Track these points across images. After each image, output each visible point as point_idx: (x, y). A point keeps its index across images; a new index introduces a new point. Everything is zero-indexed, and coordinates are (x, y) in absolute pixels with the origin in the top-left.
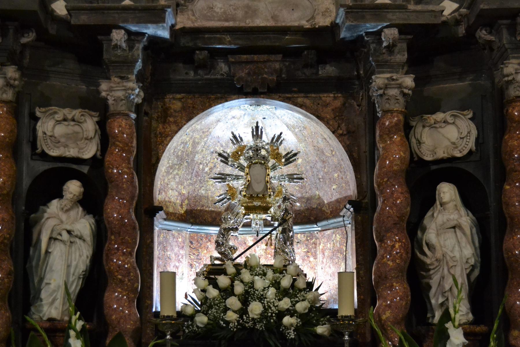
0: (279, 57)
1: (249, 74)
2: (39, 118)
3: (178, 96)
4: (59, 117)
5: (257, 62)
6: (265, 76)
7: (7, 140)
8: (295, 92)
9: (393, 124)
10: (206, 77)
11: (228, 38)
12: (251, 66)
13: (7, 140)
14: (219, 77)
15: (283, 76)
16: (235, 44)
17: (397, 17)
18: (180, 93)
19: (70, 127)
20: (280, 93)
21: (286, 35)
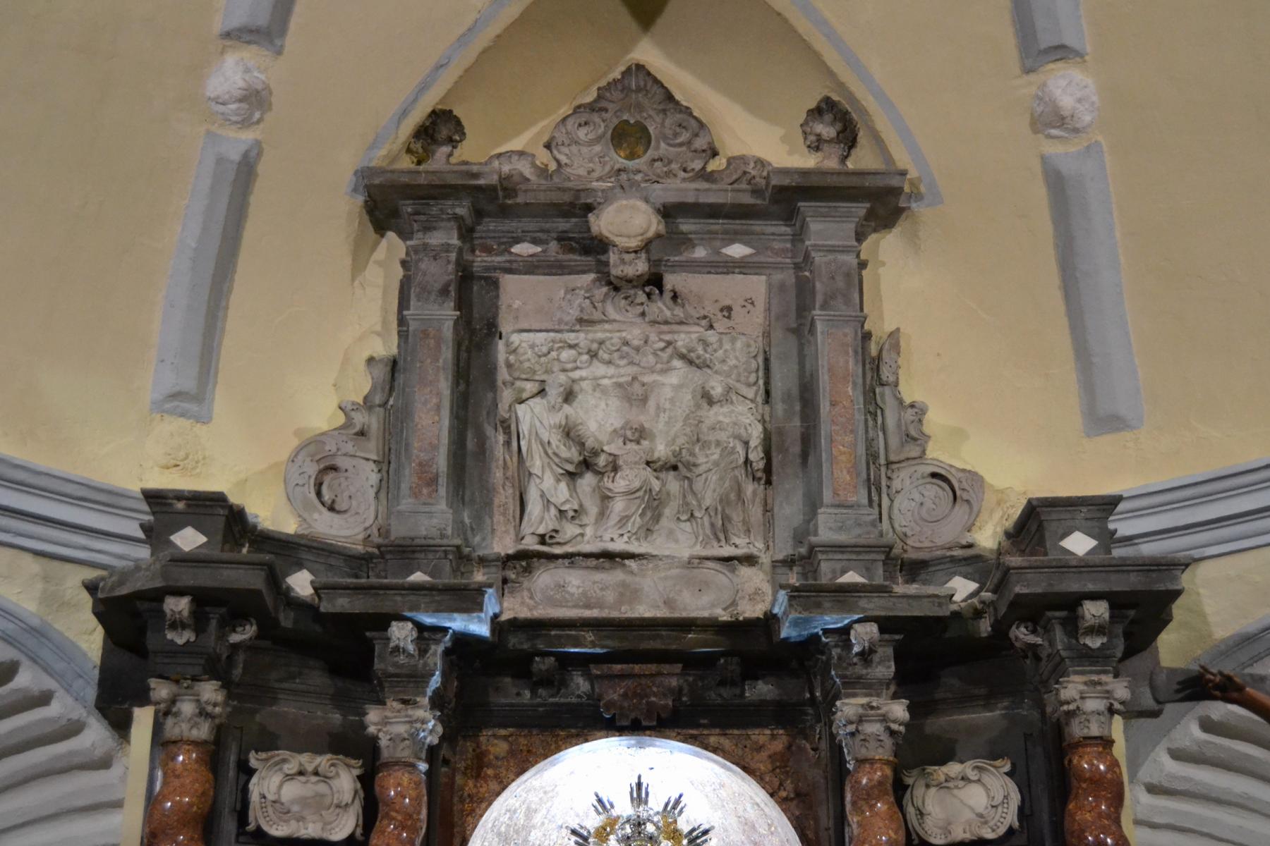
0: (678, 668)
1: (625, 695)
2: (255, 770)
3: (503, 732)
4: (291, 767)
5: (639, 676)
6: (653, 699)
7: (195, 809)
8: (704, 726)
9: (875, 782)
10: (552, 700)
11: (590, 636)
12: (629, 683)
13: (195, 809)
14: (574, 700)
15: (684, 699)
16: (603, 647)
17: (876, 606)
18: (505, 726)
19: (309, 785)
20: (678, 727)
21: (689, 632)
